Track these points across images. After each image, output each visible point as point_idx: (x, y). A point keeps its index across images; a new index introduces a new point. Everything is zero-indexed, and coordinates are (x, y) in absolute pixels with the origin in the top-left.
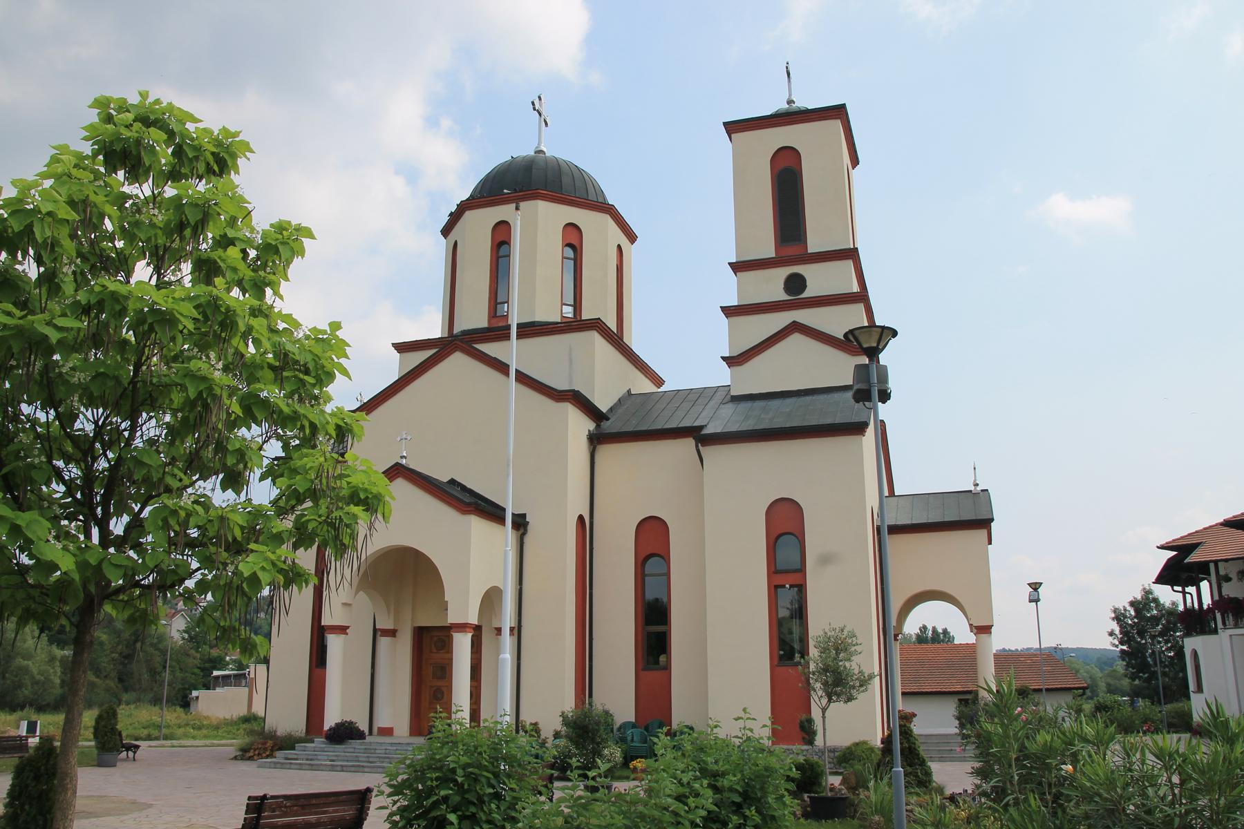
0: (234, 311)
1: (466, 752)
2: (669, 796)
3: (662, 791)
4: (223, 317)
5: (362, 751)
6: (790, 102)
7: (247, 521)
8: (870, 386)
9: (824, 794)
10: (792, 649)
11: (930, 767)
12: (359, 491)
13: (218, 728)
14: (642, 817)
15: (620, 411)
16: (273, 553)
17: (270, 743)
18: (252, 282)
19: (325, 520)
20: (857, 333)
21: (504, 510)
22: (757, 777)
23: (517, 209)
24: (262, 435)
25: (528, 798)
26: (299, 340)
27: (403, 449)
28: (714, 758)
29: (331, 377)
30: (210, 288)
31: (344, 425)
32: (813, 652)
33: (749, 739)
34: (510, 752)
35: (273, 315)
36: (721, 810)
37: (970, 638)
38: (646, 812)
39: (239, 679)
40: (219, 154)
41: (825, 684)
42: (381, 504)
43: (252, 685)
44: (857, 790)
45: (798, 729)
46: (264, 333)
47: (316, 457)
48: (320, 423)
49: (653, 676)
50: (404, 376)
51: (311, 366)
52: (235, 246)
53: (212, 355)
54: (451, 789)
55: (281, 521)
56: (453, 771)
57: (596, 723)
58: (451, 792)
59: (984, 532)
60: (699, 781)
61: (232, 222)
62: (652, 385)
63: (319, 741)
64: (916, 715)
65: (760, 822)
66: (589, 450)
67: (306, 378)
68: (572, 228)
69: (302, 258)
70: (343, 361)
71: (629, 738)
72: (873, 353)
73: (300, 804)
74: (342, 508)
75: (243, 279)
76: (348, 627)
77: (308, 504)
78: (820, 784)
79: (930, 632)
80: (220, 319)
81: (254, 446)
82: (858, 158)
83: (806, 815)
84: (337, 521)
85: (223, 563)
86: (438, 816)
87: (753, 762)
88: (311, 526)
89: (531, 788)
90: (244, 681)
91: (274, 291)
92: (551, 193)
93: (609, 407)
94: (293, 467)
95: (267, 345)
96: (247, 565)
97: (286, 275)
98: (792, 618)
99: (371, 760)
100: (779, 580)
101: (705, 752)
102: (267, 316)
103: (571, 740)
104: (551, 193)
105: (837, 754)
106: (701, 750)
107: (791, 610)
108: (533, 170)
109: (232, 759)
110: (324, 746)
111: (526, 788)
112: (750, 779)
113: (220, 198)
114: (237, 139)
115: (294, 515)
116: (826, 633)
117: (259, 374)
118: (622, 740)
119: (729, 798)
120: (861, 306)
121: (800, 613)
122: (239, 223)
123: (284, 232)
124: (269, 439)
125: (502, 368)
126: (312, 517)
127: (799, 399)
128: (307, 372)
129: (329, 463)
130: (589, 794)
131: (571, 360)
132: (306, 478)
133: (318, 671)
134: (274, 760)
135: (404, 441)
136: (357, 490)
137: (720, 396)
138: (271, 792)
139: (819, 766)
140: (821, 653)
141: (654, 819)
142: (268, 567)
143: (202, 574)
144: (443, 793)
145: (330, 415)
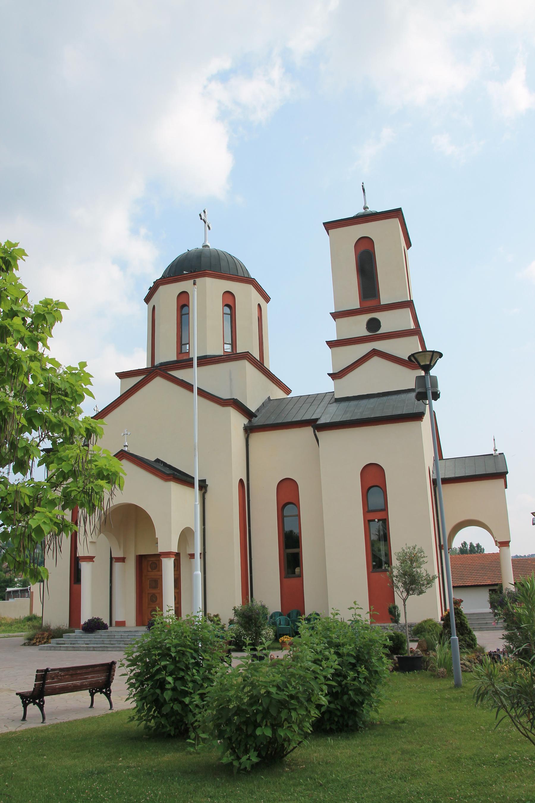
0: (20, 358)
1: (176, 636)
2: (309, 661)
3: (305, 658)
4: (13, 362)
5: (106, 637)
6: (365, 208)
7: (33, 492)
8: (426, 390)
9: (407, 655)
10: (380, 560)
11: (474, 635)
12: (103, 470)
13: (12, 625)
14: (293, 675)
15: (264, 411)
16: (50, 512)
17: (46, 634)
18: (30, 339)
19: (82, 490)
20: (416, 356)
21: (193, 478)
22: (364, 645)
23: (194, 284)
24: (39, 436)
25: (218, 665)
26: (60, 375)
27: (126, 441)
28: (336, 635)
29: (82, 397)
30: (5, 344)
31: (91, 428)
32: (395, 562)
33: (357, 621)
34: (204, 635)
35: (43, 360)
36: (342, 668)
37: (496, 550)
38: (295, 672)
39: (24, 593)
40: (5, 258)
41: (405, 583)
42: (118, 479)
43: (31, 597)
44: (428, 651)
45: (388, 614)
46: (38, 372)
47: (74, 449)
48: (76, 427)
49: (293, 581)
50: (125, 393)
51: (69, 391)
52: (18, 316)
53: (7, 387)
54: (168, 661)
55: (54, 491)
56: (169, 649)
57: (256, 614)
58: (168, 663)
59: (502, 481)
60: (328, 650)
61: (15, 301)
62: (284, 393)
63: (78, 632)
64: (463, 601)
65: (368, 675)
66: (245, 436)
67: (66, 398)
68: (228, 294)
69: (61, 322)
70: (88, 387)
71: (278, 623)
72: (427, 368)
73: (70, 673)
74: (93, 482)
75: (24, 337)
76: (94, 557)
77: (70, 480)
78: (404, 649)
79: (469, 546)
80: (11, 364)
81: (34, 444)
82: (410, 243)
83: (395, 669)
84: (90, 490)
85: (18, 521)
86: (160, 678)
87: (361, 636)
88: (73, 494)
89: (219, 658)
90: (27, 594)
91: (43, 344)
92: (213, 272)
93: (257, 409)
94: (59, 457)
95: (40, 379)
96: (34, 522)
97: (51, 333)
98: (380, 540)
99: (112, 642)
100: (371, 516)
101: (331, 631)
102: (39, 361)
103: (241, 625)
104: (213, 272)
105: (413, 628)
106: (328, 629)
107: (379, 535)
108: (202, 258)
109: (22, 645)
110: (81, 634)
111: (216, 659)
112: (360, 647)
113: (8, 286)
114: (16, 248)
115: (62, 488)
116: (404, 550)
117: (36, 398)
118: (274, 624)
119: (347, 660)
120: (417, 338)
121: (385, 537)
122: (20, 302)
123: (49, 306)
124: (43, 438)
125: (189, 387)
126: (74, 489)
127: (379, 399)
128: (66, 395)
129: (83, 453)
130: (258, 661)
131: (231, 380)
132: (69, 463)
133: (75, 586)
134: (49, 645)
135: (126, 436)
136: (102, 470)
137: (327, 399)
138: (51, 667)
139: (403, 637)
140: (401, 563)
141: (300, 676)
142: (48, 521)
143: (4, 528)
144: (163, 663)
145: (81, 422)
